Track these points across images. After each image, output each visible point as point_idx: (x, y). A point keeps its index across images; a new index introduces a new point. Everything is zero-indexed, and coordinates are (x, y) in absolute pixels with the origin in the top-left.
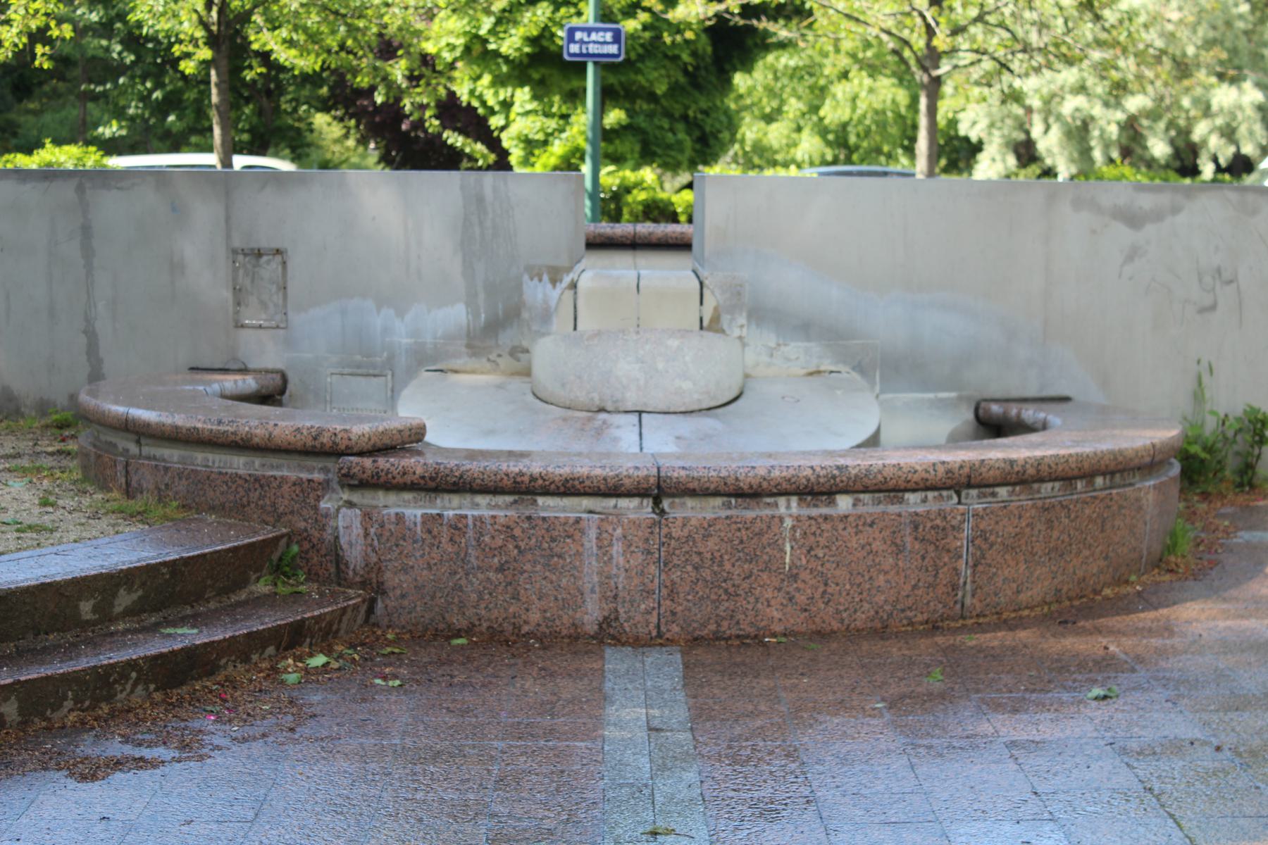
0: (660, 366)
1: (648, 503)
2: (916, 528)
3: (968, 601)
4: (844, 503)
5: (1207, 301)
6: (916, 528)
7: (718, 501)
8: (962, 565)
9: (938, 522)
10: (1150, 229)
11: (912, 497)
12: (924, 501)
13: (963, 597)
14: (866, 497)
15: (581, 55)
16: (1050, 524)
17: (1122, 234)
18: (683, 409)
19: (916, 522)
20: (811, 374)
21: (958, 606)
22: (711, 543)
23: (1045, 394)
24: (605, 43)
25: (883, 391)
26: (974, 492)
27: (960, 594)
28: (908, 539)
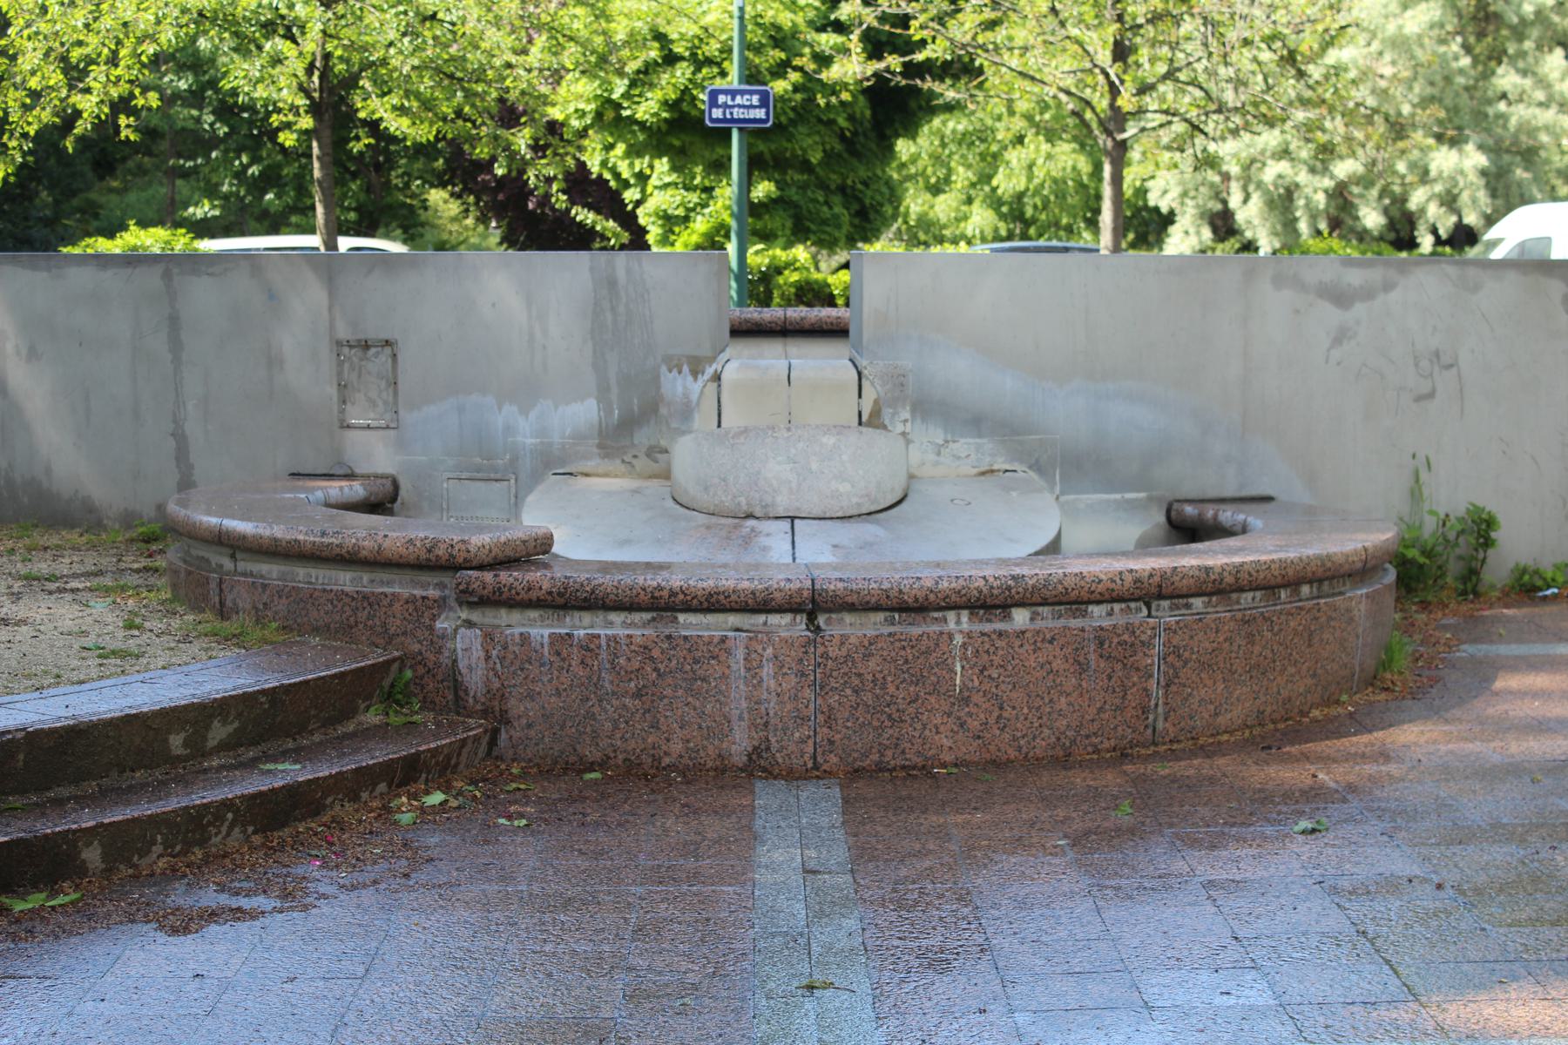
0: (814, 466)
2: (1101, 644)
3: (1160, 725)
5: (1425, 387)
6: (1101, 644)
8: (1152, 685)
9: (1126, 637)
10: (1359, 309)
11: (1096, 610)
12: (1110, 614)
14: (1045, 610)
15: (725, 120)
17: (1330, 314)
18: (817, 512)
20: (983, 473)
21: (1149, 731)
23: (1244, 493)
24: (752, 107)
25: (1063, 493)
27: (1151, 717)
28: (1092, 657)
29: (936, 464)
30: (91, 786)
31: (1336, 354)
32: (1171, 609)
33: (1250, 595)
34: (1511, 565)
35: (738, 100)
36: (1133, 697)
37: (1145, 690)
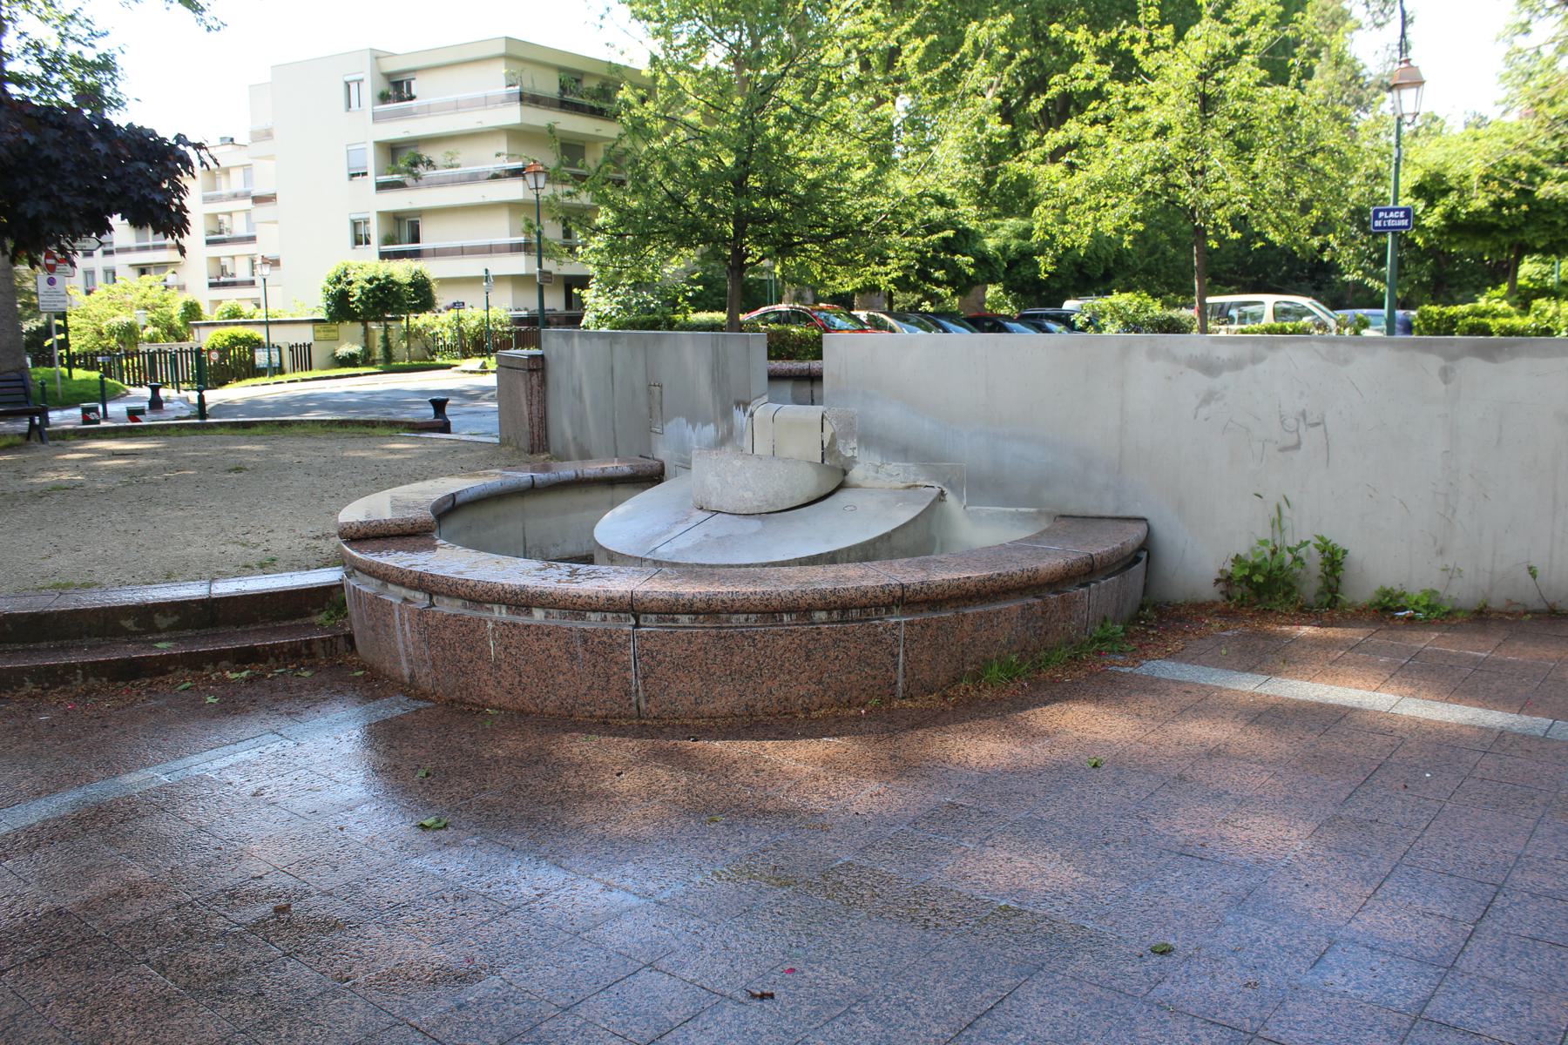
0: (729, 479)
1: (427, 596)
2: (586, 641)
3: (643, 705)
4: (538, 615)
5: (1291, 440)
6: (586, 641)
7: (459, 602)
8: (631, 675)
9: (605, 639)
10: (1227, 377)
11: (593, 616)
12: (604, 619)
13: (638, 701)
14: (555, 612)
15: (1382, 227)
16: (729, 651)
17: (1202, 382)
18: (731, 510)
19: (585, 637)
20: (909, 487)
21: (634, 708)
22: (448, 632)
23: (1120, 514)
24: (1399, 219)
25: (969, 504)
26: (653, 617)
27: (634, 699)
28: (580, 650)
29: (876, 479)
30: (252, 627)
31: (1204, 412)
32: (657, 621)
33: (742, 617)
34: (1377, 587)
35: (1391, 215)
36: (615, 683)
37: (625, 678)
